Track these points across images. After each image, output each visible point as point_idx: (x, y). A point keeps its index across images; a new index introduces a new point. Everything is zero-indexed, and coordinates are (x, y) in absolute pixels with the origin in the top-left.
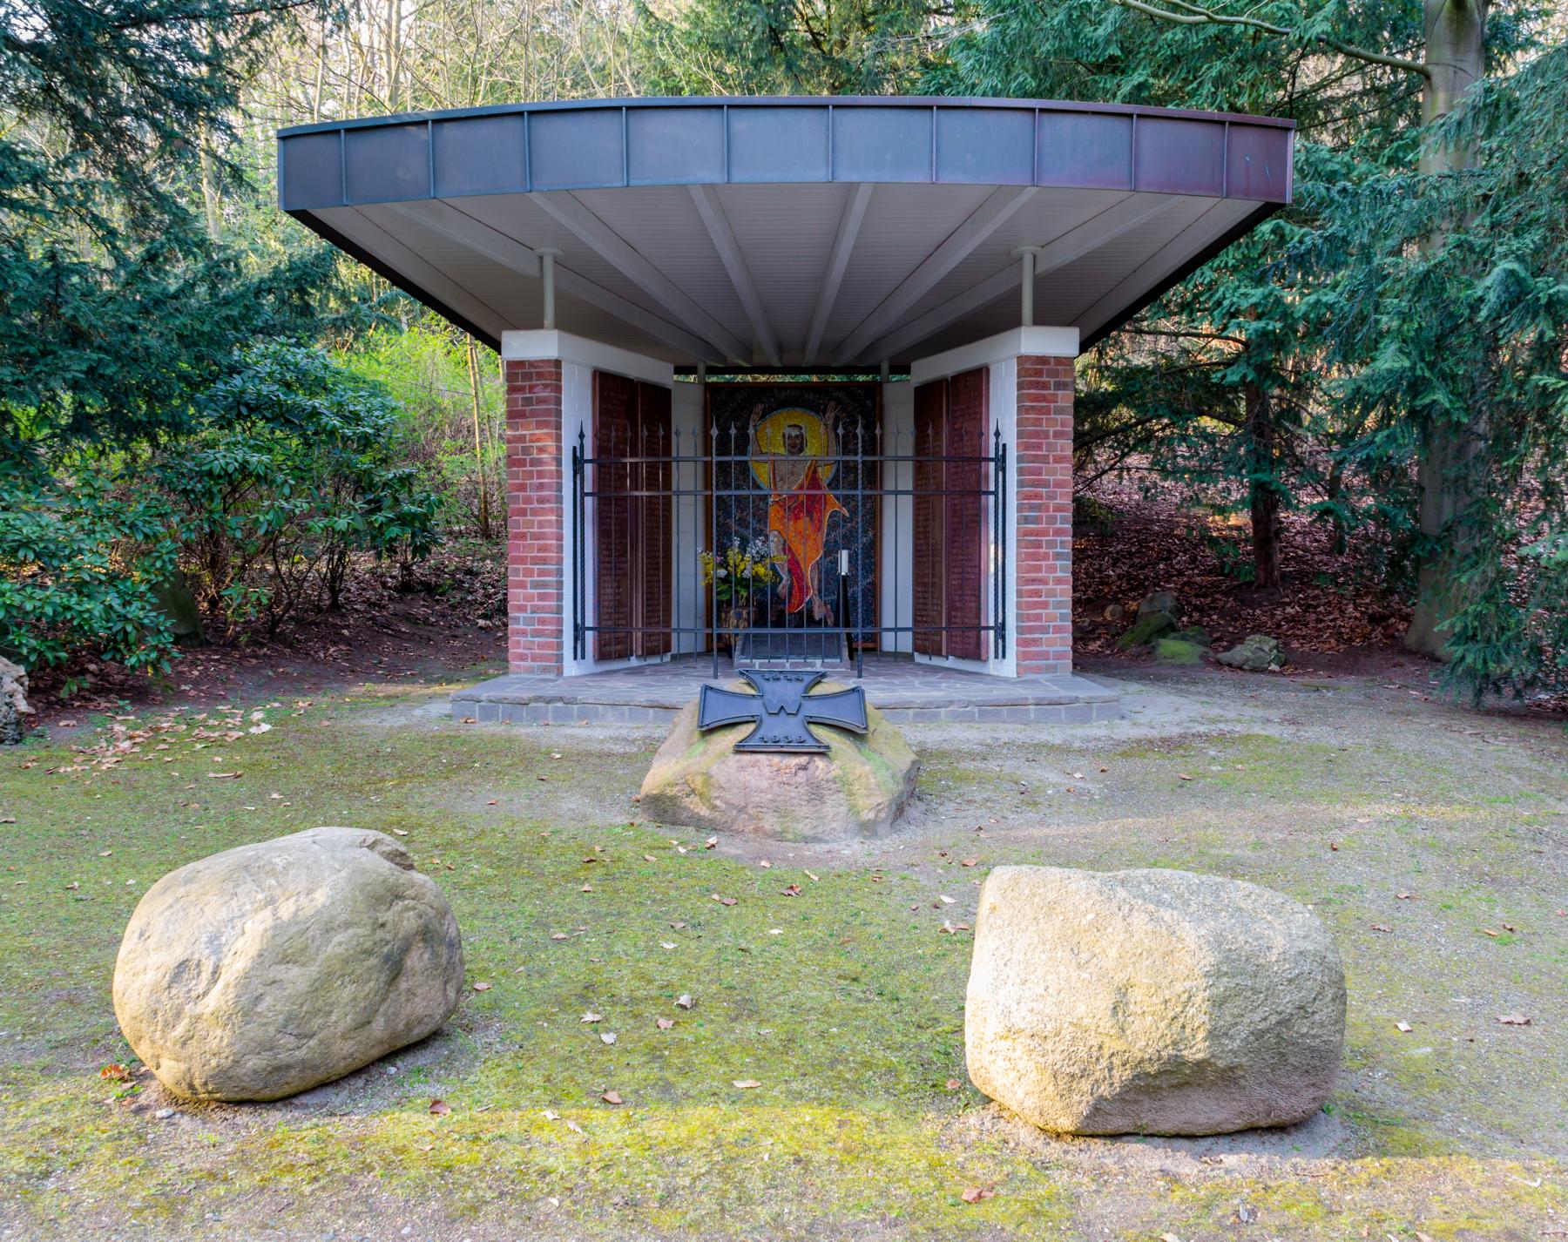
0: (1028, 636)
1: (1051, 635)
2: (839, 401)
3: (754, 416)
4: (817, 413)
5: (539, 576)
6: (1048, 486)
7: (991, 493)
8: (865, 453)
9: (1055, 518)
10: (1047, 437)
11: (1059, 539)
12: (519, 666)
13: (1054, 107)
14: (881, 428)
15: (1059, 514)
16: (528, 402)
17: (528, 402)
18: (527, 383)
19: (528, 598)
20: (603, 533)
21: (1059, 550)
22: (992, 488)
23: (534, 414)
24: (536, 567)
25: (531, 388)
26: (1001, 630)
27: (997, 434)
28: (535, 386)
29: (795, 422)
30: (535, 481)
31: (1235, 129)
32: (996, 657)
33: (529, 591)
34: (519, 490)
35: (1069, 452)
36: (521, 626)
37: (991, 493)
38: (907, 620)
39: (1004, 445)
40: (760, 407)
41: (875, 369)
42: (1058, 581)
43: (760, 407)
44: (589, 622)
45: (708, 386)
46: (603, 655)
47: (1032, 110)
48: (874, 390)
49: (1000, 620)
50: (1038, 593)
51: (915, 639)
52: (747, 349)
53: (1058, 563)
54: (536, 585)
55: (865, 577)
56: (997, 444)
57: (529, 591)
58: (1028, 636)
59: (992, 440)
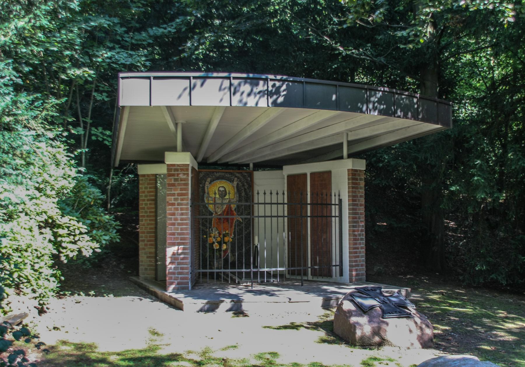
1: (360, 267)
2: (238, 178)
3: (207, 183)
4: (231, 182)
6: (358, 215)
9: (145, 189)
10: (358, 197)
13: (343, 85)
16: (176, 180)
17: (176, 180)
20: (329, 252)
23: (179, 185)
25: (178, 175)
28: (179, 174)
29: (223, 185)
35: (363, 203)
40: (209, 179)
42: (144, 200)
43: (209, 179)
47: (336, 86)
50: (356, 253)
55: (246, 230)
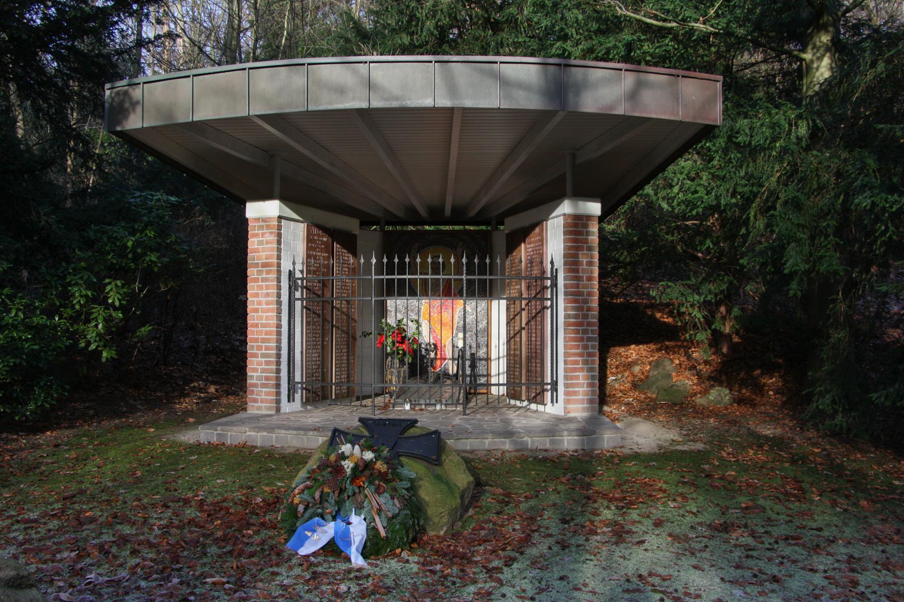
0: (571, 389)
5: (265, 350)
7: (549, 299)
8: (467, 274)
11: (590, 328)
12: (253, 406)
14: (490, 258)
15: (264, 269)
18: (260, 232)
19: (259, 364)
21: (590, 335)
22: (549, 297)
24: (264, 344)
25: (263, 234)
26: (554, 385)
27: (552, 263)
30: (265, 291)
31: (626, 72)
32: (552, 402)
33: (260, 359)
34: (255, 297)
36: (254, 381)
37: (549, 299)
38: (503, 379)
39: (556, 270)
41: (487, 223)
44: (298, 378)
45: (386, 234)
46: (306, 402)
48: (487, 235)
49: (555, 379)
51: (507, 389)
52: (412, 210)
53: (590, 343)
54: (263, 356)
56: (552, 269)
57: (260, 359)
58: (571, 389)
59: (549, 266)
